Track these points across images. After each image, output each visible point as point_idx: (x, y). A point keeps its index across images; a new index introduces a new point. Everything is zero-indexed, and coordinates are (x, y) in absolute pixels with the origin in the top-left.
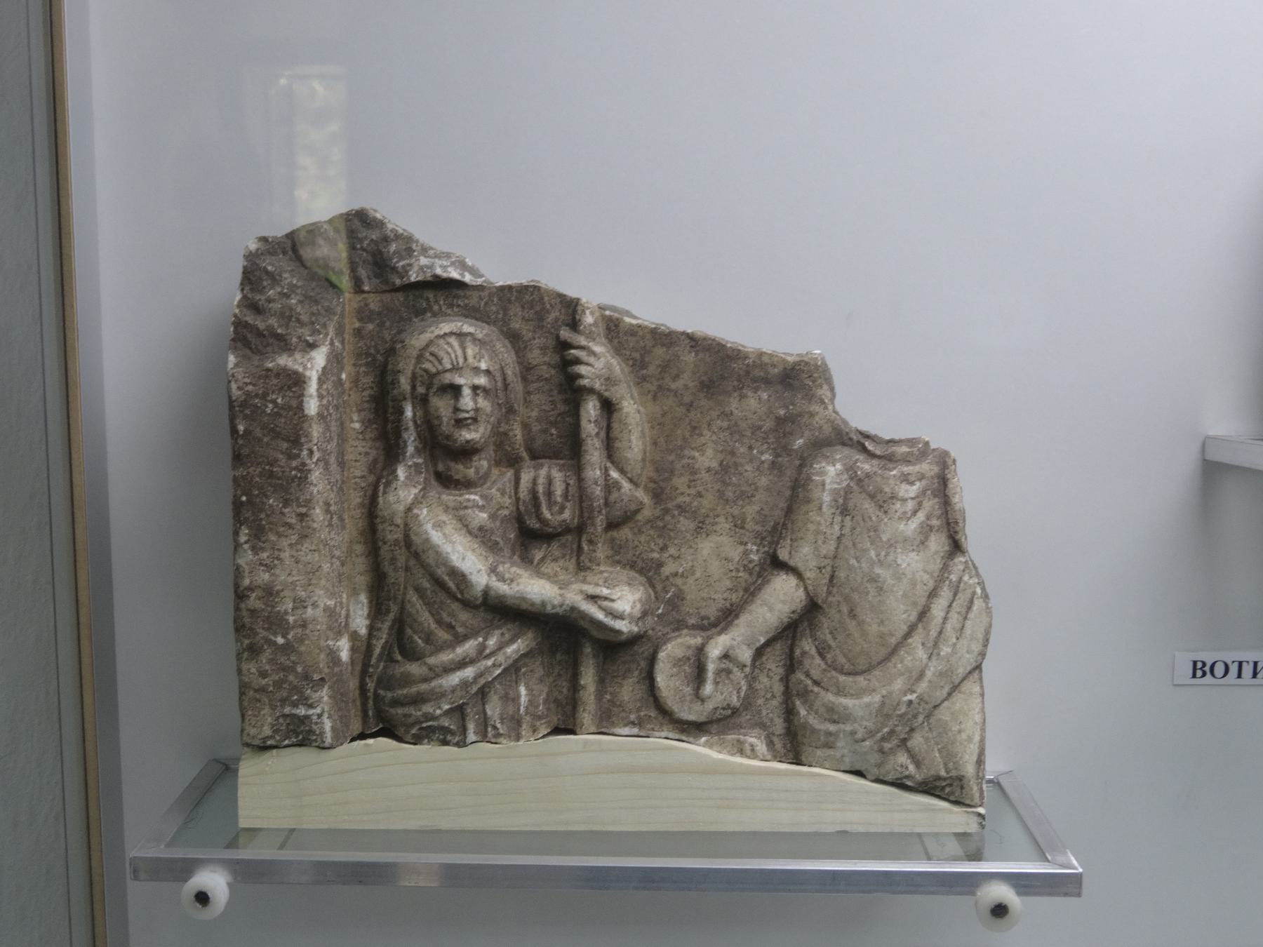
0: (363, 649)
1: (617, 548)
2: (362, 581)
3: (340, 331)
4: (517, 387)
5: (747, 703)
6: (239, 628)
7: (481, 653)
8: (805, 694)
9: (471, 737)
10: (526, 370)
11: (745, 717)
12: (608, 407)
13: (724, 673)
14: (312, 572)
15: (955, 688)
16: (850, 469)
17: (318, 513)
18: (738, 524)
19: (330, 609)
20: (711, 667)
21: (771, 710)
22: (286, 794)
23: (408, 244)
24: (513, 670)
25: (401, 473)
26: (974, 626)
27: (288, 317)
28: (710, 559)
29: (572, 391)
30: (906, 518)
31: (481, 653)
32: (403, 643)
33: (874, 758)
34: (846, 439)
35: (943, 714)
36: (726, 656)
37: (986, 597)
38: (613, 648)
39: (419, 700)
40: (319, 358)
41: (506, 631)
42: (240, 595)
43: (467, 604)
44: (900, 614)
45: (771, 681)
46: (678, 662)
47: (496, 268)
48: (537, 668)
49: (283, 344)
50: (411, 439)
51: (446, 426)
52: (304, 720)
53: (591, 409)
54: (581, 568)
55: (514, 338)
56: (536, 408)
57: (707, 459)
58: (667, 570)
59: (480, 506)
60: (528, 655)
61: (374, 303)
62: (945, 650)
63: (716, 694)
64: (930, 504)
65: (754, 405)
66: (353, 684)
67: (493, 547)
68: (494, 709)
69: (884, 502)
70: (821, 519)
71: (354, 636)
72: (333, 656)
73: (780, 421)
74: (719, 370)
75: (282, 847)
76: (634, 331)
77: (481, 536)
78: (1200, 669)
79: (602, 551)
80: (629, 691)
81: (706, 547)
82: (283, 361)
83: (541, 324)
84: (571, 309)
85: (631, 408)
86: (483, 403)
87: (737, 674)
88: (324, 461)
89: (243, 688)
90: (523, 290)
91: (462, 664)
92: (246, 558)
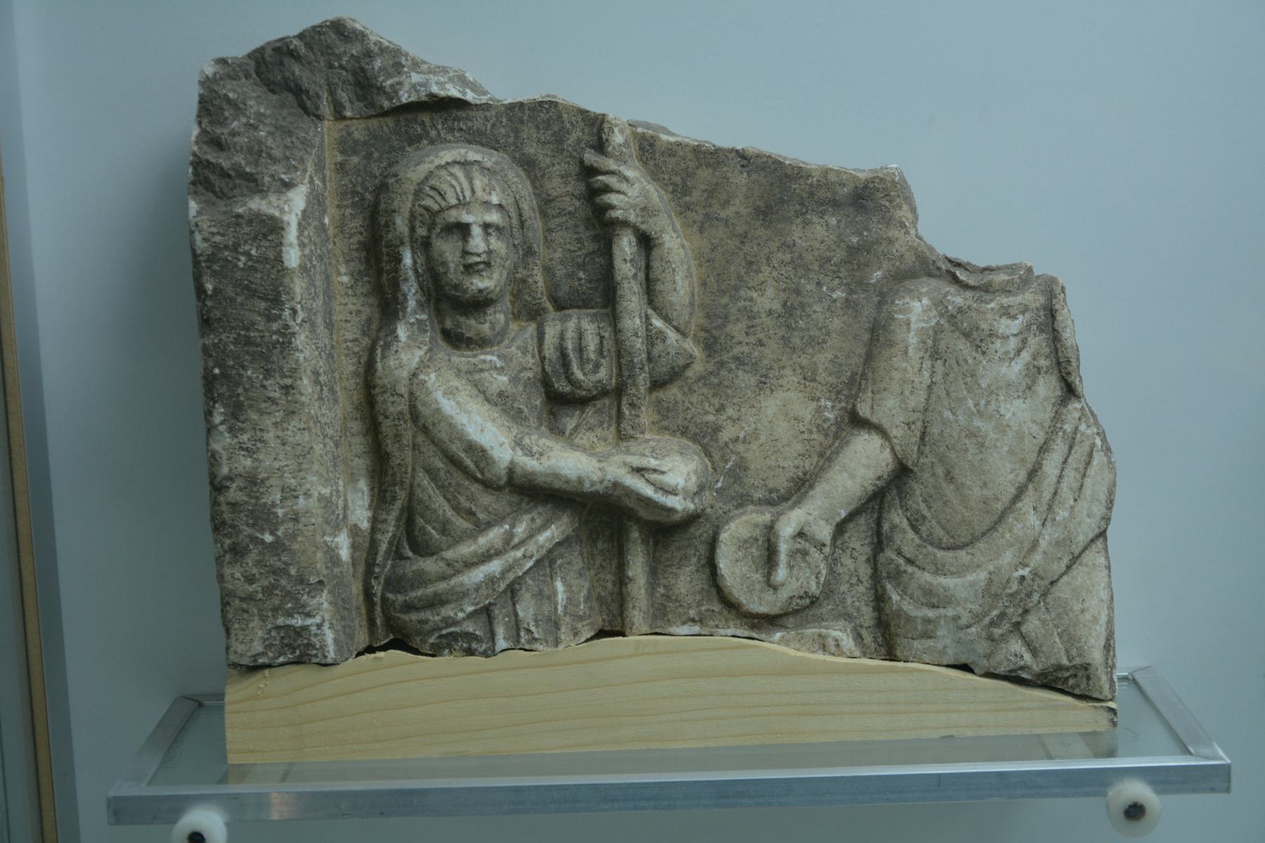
19: (327, 502)
21: (857, 597)
23: (396, 60)
24: (547, 562)
26: (1096, 484)
28: (777, 418)
29: (602, 225)
38: (665, 531)
44: (1006, 475)
45: (855, 562)
47: (500, 81)
49: (255, 185)
53: (626, 245)
56: (560, 249)
57: (767, 300)
63: (793, 580)
69: (979, 339)
74: (780, 190)
77: (501, 402)
83: (565, 148)
84: (597, 128)
85: (675, 243)
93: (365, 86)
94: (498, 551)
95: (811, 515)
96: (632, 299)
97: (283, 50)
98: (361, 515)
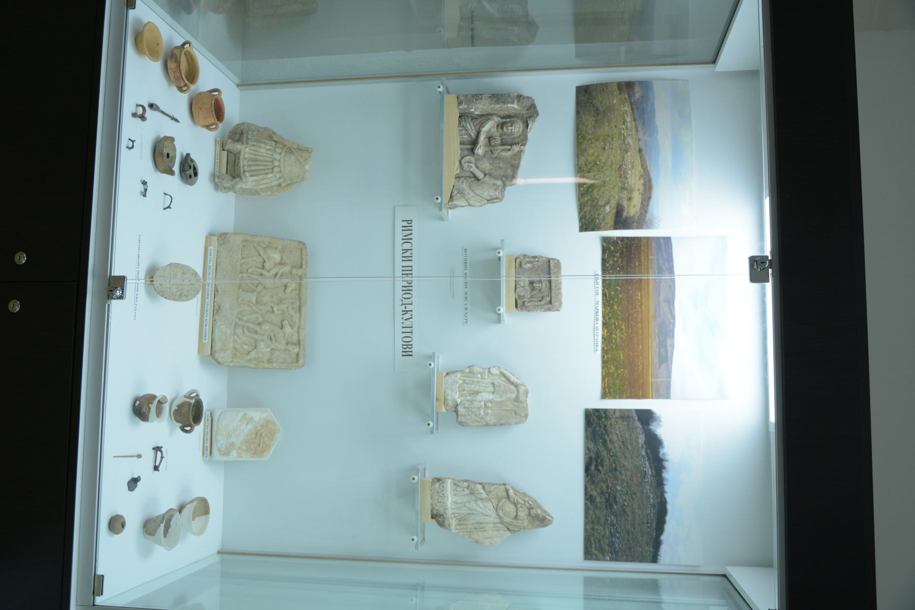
0: (472, 113)
19: (477, 109)
21: (462, 174)
22: (451, 100)
23: (534, 121)
24: (469, 135)
26: (476, 204)
28: (486, 165)
29: (511, 145)
34: (504, 186)
38: (472, 151)
44: (478, 192)
45: (468, 174)
47: (530, 135)
49: (518, 102)
53: (509, 147)
56: (509, 140)
57: (501, 165)
63: (465, 166)
65: (510, 172)
69: (495, 189)
70: (492, 181)
74: (515, 167)
77: (490, 130)
80: (466, 153)
83: (522, 140)
84: (524, 145)
85: (509, 153)
93: (530, 117)
94: (471, 128)
95: (474, 169)
96: (502, 148)
97: (535, 107)
98: (477, 113)
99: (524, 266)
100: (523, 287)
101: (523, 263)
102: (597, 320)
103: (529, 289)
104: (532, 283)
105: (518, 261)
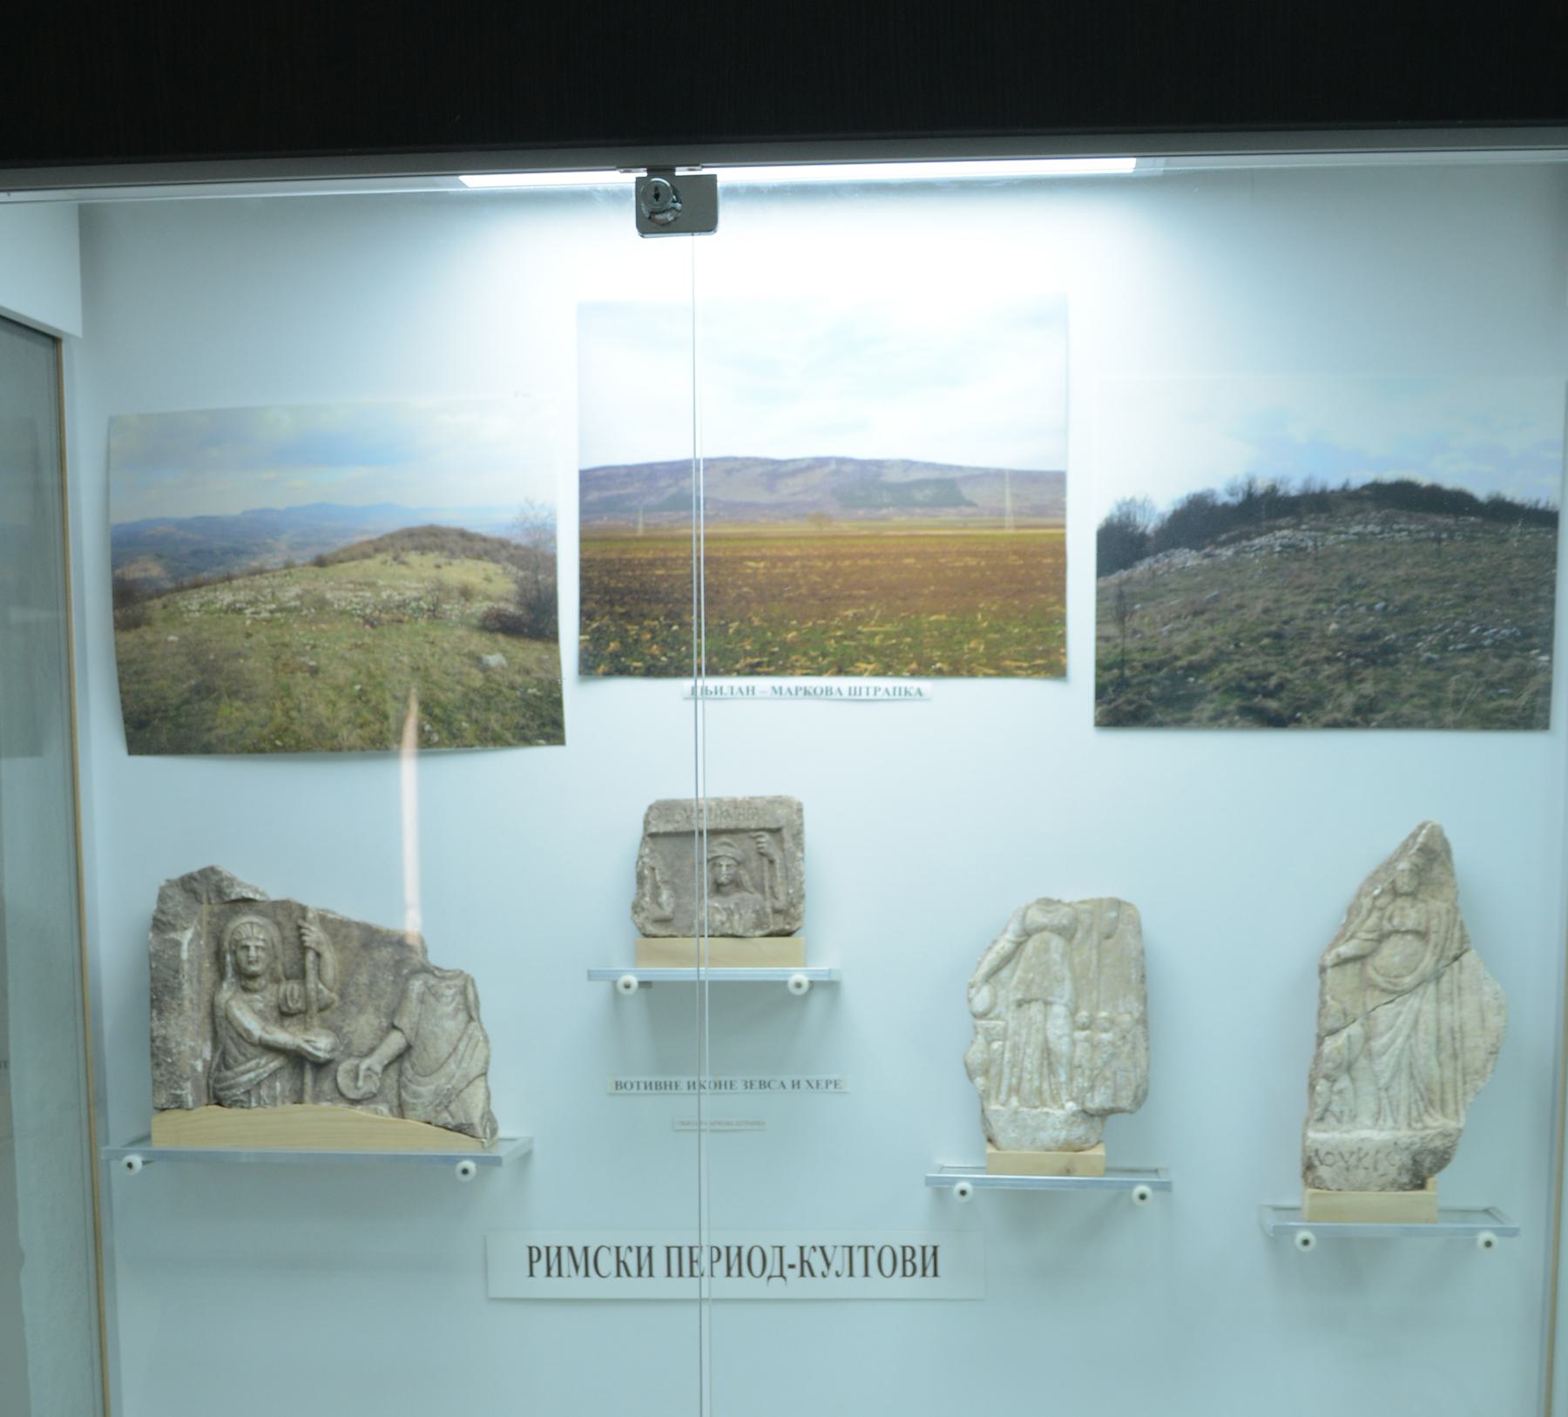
0: (208, 1066)
1: (323, 1020)
2: (209, 1035)
3: (200, 922)
4: (279, 947)
5: (380, 1091)
6: (153, 1055)
7: (258, 1066)
8: (405, 1087)
9: (254, 1104)
10: (284, 939)
11: (379, 1098)
12: (318, 955)
13: (367, 1077)
14: (184, 1030)
15: (470, 1083)
16: (426, 983)
17: (187, 1003)
18: (377, 1009)
19: (195, 1051)
20: (361, 1074)
22: (170, 1131)
23: (232, 882)
24: (273, 1075)
25: (225, 985)
26: (480, 1054)
27: (176, 916)
28: (364, 1024)
30: (448, 1004)
31: (258, 1066)
32: (224, 1061)
33: (433, 1115)
34: (426, 969)
35: (464, 1095)
36: (369, 1069)
37: (486, 1040)
38: (321, 1066)
39: (230, 1088)
40: (189, 934)
41: (270, 1056)
42: (153, 1040)
43: (252, 1044)
44: (445, 1049)
45: (392, 1079)
46: (348, 1072)
47: (274, 892)
48: (286, 1073)
49: (174, 928)
50: (230, 971)
51: (244, 964)
52: (179, 1096)
53: (310, 956)
54: (306, 1029)
55: (278, 924)
56: (287, 956)
57: (363, 979)
58: (345, 1030)
59: (259, 1001)
60: (281, 1068)
61: (217, 909)
62: (464, 1065)
63: (365, 1086)
64: (459, 998)
65: (385, 954)
66: (204, 1082)
67: (265, 1019)
68: (264, 1092)
69: (437, 996)
70: (412, 1005)
71: (204, 1061)
72: (194, 1069)
73: (397, 962)
75: (1349, 1037)
76: (332, 921)
77: (260, 1014)
78: (619, 1085)
79: (316, 1021)
80: (327, 1086)
81: (362, 1020)
82: (173, 935)
83: (289, 915)
84: (303, 910)
85: (329, 956)
86: (261, 954)
87: (375, 1078)
88: (190, 980)
89: (154, 1081)
90: (283, 902)
91: (249, 1071)
92: (156, 1023)
99: (668, 911)
100: (730, 913)
101: (658, 913)
102: (828, 691)
103: (736, 897)
104: (718, 888)
105: (651, 929)
